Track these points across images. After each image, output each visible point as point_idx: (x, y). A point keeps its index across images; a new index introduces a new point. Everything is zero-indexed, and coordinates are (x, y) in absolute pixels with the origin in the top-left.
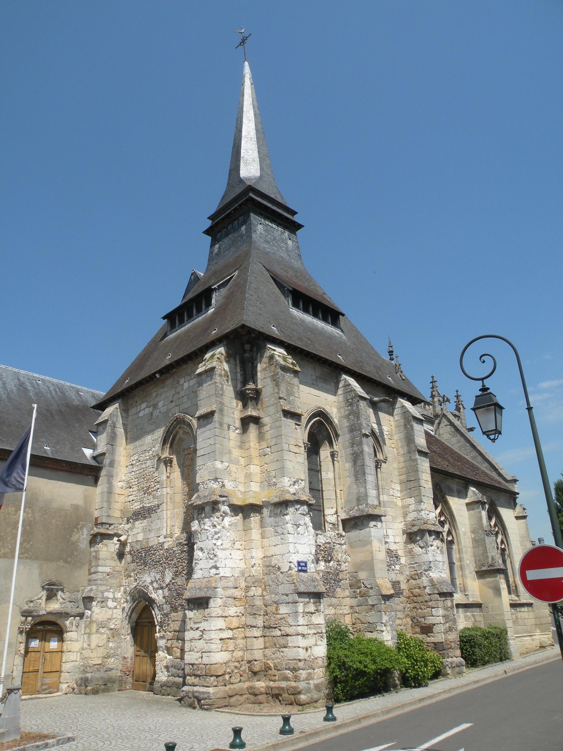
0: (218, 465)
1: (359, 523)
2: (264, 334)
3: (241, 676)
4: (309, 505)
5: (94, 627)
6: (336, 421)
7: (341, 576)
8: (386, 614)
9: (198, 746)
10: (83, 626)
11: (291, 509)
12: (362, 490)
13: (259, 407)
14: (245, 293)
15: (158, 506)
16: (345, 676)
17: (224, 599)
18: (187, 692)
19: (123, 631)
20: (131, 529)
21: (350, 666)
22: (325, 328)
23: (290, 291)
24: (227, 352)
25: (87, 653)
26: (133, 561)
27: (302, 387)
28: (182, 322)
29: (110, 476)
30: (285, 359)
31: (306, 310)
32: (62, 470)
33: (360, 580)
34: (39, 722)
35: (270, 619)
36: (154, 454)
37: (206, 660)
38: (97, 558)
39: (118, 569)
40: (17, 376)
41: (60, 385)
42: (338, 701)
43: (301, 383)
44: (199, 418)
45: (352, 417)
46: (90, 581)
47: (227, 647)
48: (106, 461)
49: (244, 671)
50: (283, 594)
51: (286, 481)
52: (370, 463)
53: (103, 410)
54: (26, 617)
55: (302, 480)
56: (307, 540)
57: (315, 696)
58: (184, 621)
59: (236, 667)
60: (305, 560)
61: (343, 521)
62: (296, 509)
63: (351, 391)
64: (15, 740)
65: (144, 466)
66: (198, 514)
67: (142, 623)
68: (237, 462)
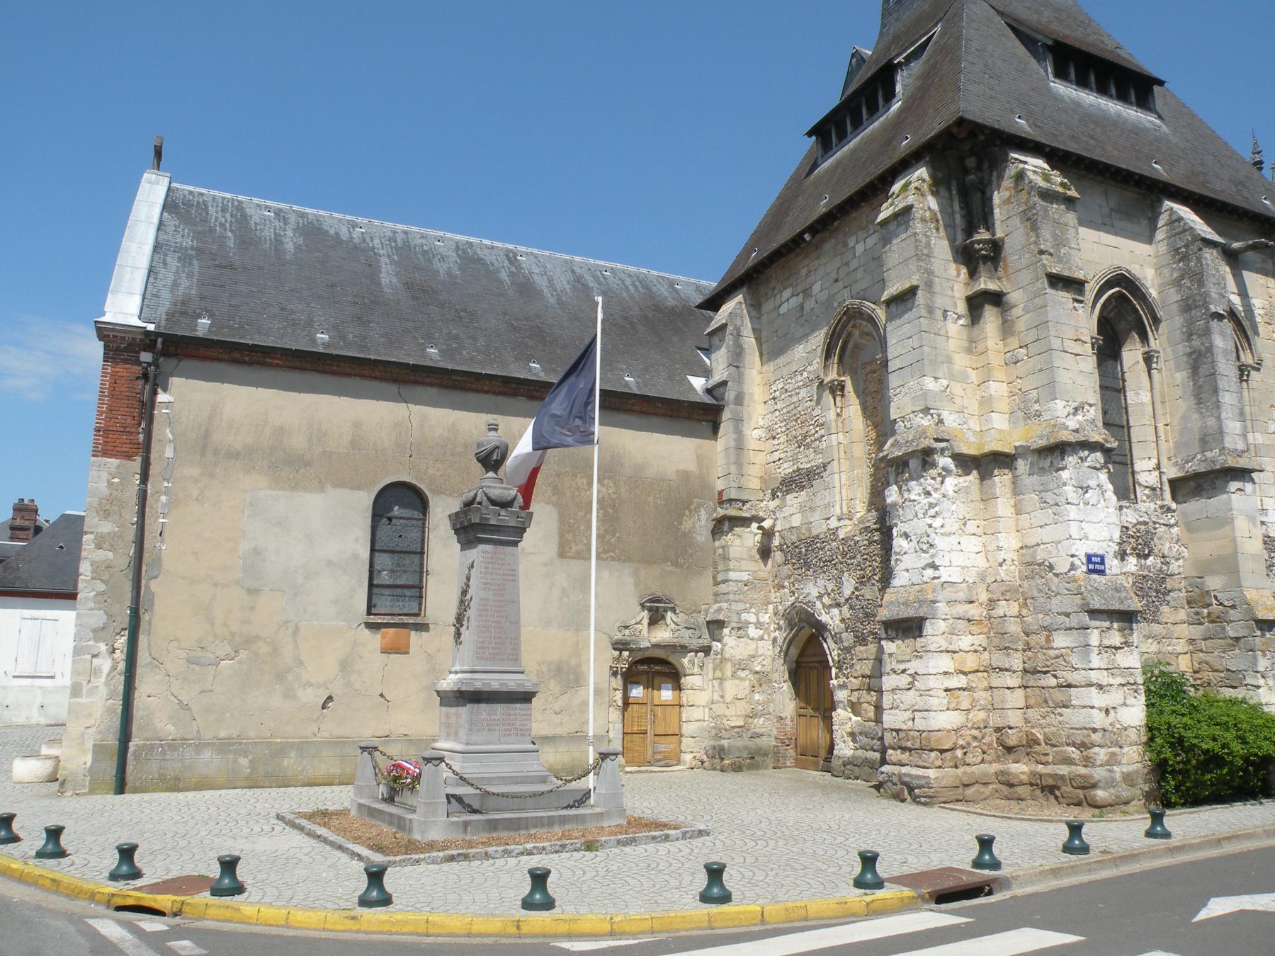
0: (929, 383)
1: (1205, 486)
2: (1003, 132)
3: (984, 753)
4: (1107, 452)
5: (729, 670)
6: (1153, 293)
7: (1169, 584)
8: (1264, 655)
9: (916, 860)
10: (711, 666)
11: (1070, 459)
12: (1211, 422)
13: (1001, 272)
14: (959, 61)
15: (825, 466)
16: (1182, 762)
17: (951, 621)
18: (890, 775)
19: (776, 676)
20: (780, 508)
21: (1194, 745)
22: (1124, 114)
23: (1049, 48)
24: (931, 176)
25: (720, 709)
26: (786, 562)
27: (1082, 230)
28: (843, 137)
29: (738, 421)
30: (1046, 178)
31: (1082, 83)
32: (656, 414)
33: (1208, 592)
34: (654, 804)
35: (1036, 656)
36: (812, 377)
37: (920, 724)
38: (725, 558)
39: (762, 575)
40: (569, 266)
41: (642, 277)
42: (1169, 805)
43: (1082, 223)
44: (889, 303)
45: (1186, 282)
46: (716, 595)
47: (958, 703)
48: (730, 395)
49: (990, 745)
50: (1059, 614)
51: (1060, 408)
52: (1226, 369)
53: (716, 309)
54: (621, 651)
55: (1091, 405)
56: (1103, 515)
57: (1125, 793)
58: (879, 661)
59: (975, 738)
60: (1100, 552)
61: (1172, 482)
62: (1081, 458)
63: (1184, 231)
64: (620, 826)
65: (795, 399)
66: (897, 475)
67: (807, 662)
68: (963, 379)
